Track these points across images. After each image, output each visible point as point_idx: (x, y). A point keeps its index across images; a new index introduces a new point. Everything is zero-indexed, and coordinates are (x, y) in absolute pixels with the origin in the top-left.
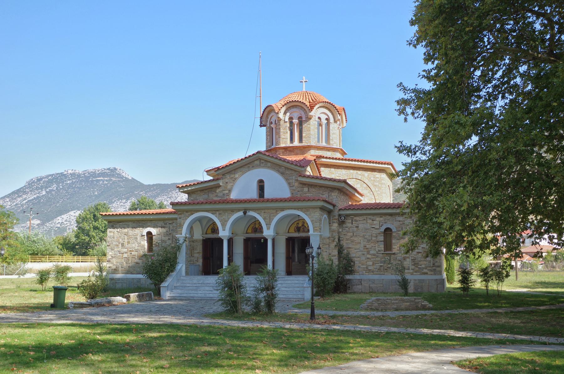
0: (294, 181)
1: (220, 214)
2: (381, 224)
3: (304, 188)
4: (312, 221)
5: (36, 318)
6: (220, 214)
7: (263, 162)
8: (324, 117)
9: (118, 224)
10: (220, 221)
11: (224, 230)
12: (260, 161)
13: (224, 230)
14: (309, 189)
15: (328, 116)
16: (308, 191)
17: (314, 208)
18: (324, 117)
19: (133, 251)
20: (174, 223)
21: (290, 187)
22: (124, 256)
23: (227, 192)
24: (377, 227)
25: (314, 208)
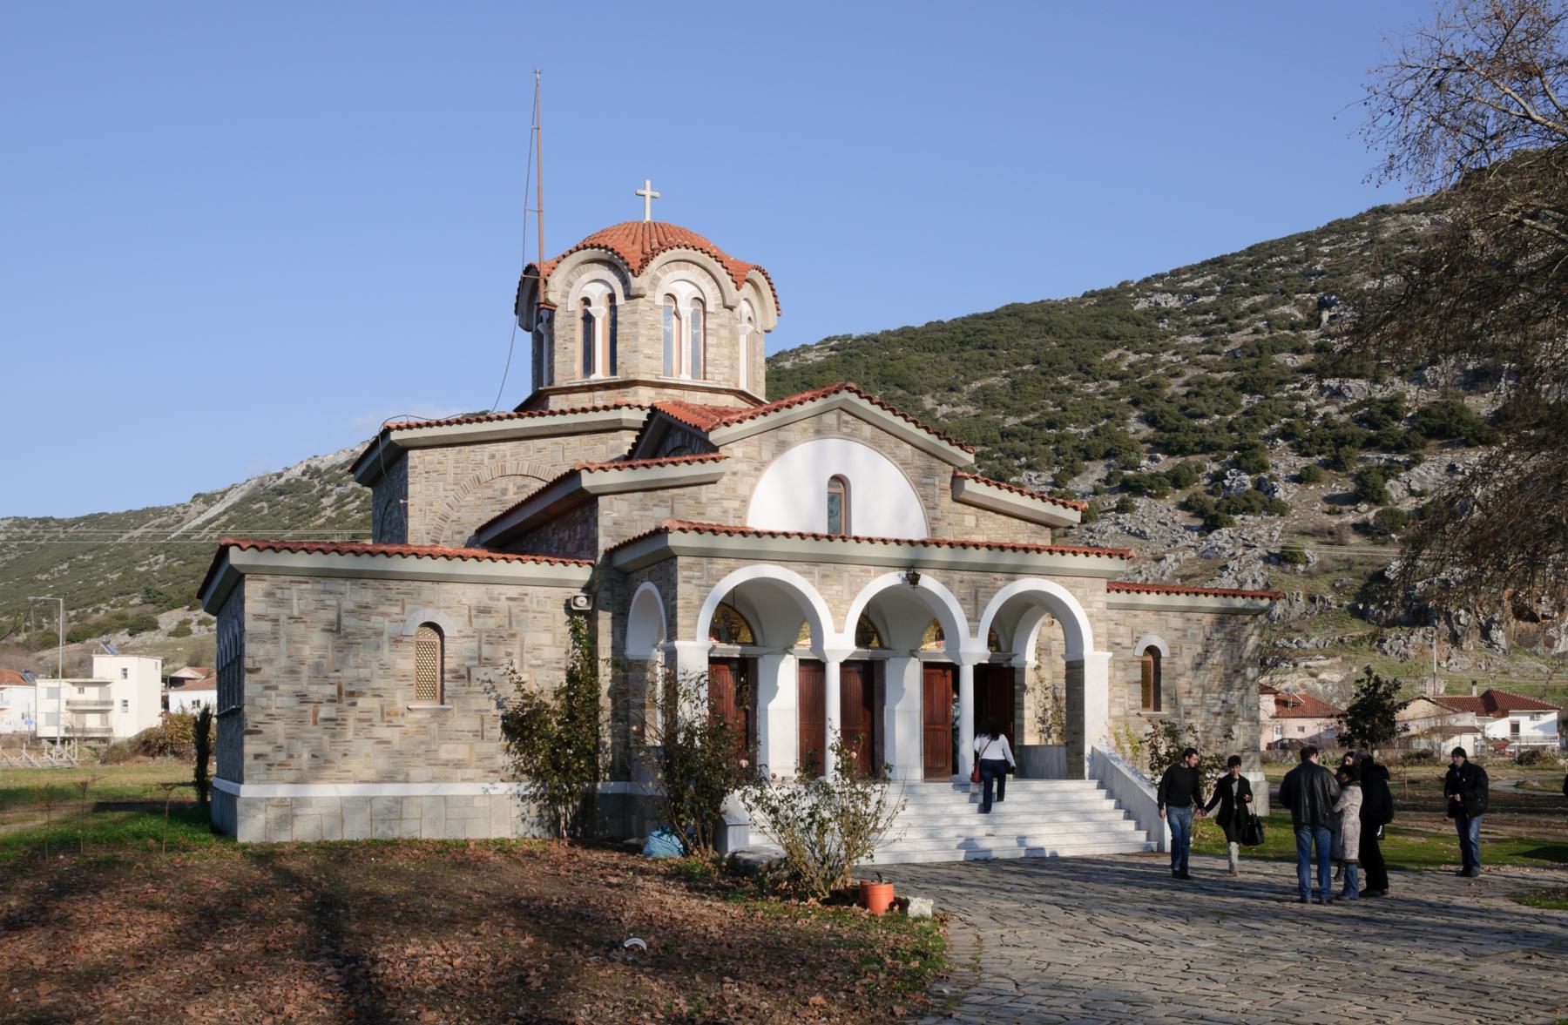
0: (937, 490)
1: (824, 576)
2: (1136, 635)
3: (967, 517)
4: (1090, 616)
5: (1051, 898)
6: (824, 576)
7: (847, 422)
8: (685, 292)
9: (295, 587)
10: (827, 601)
11: (839, 631)
12: (839, 417)
13: (839, 631)
14: (977, 520)
15: (611, 287)
16: (977, 526)
17: (1093, 575)
18: (598, 293)
19: (361, 694)
20: (527, 598)
21: (928, 508)
22: (322, 714)
23: (736, 504)
24: (1127, 642)
25: (1093, 575)
